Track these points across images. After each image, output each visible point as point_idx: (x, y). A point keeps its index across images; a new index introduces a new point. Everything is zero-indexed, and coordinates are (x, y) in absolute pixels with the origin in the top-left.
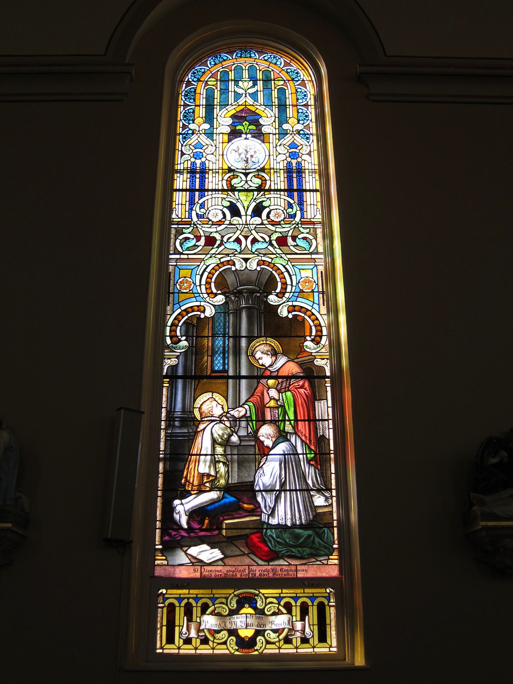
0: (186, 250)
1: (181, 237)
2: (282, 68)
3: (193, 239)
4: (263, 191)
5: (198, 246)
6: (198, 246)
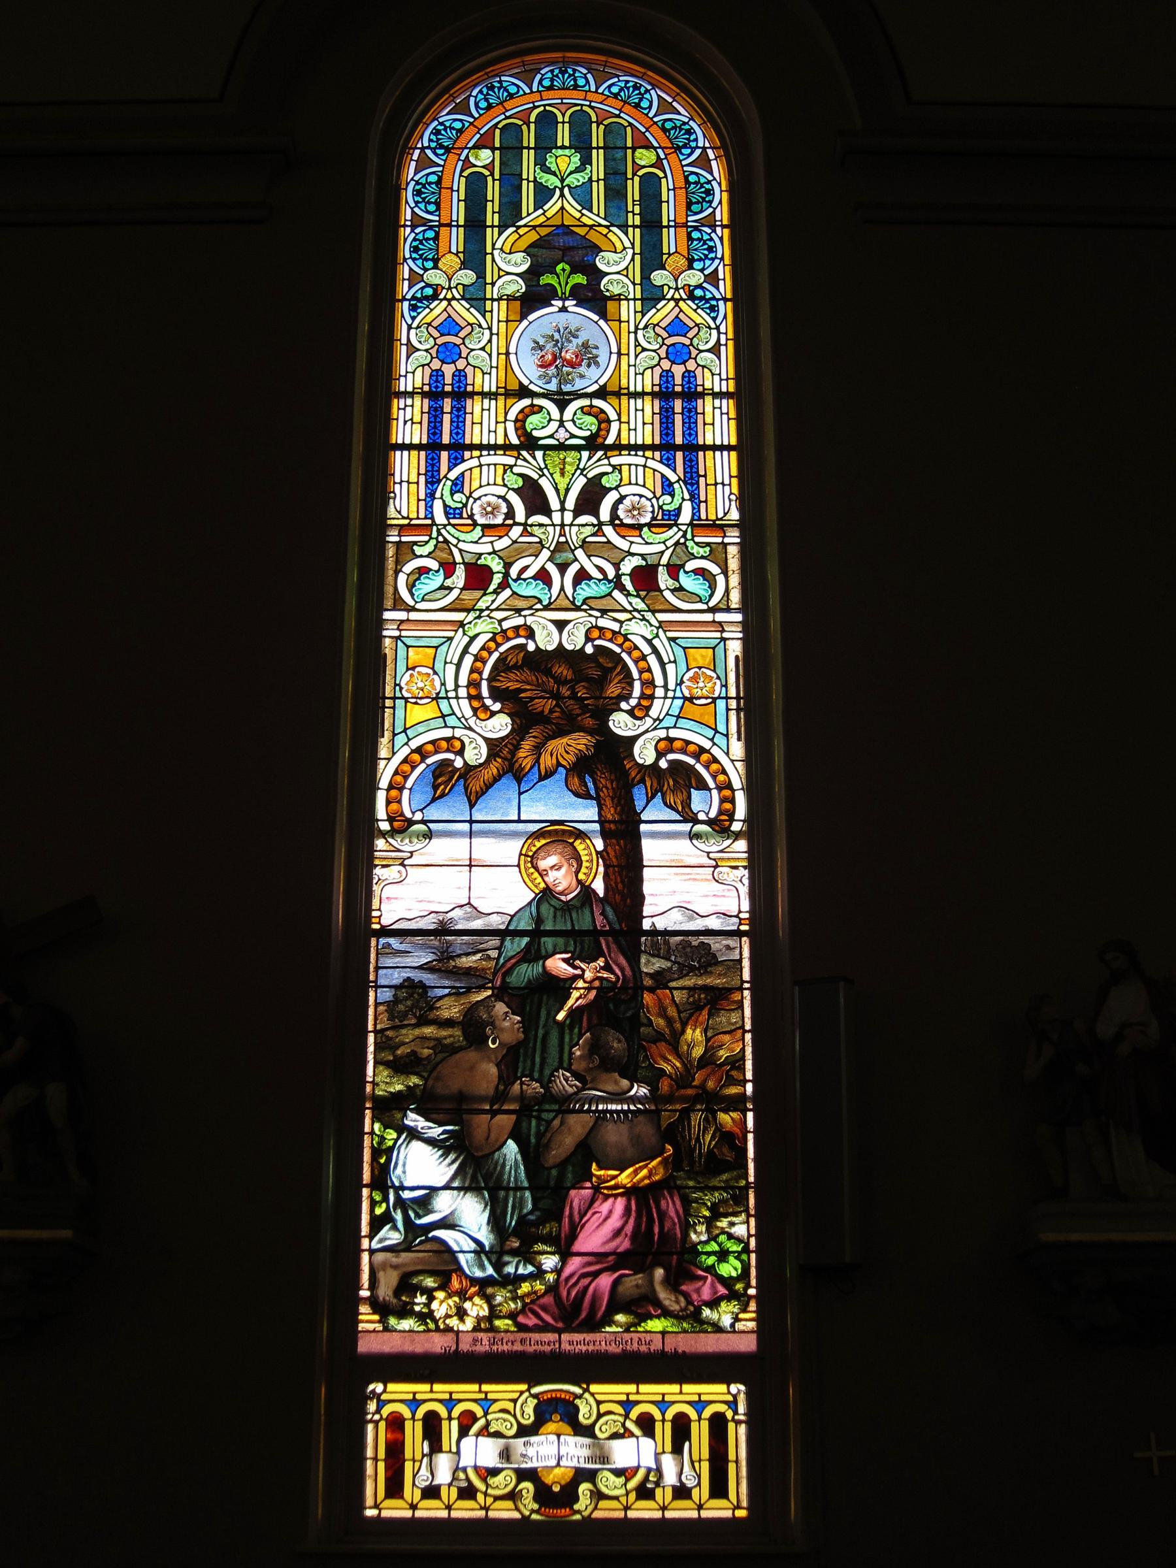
0: (423, 600)
1: (409, 567)
3: (437, 571)
5: (450, 589)
6: (450, 589)
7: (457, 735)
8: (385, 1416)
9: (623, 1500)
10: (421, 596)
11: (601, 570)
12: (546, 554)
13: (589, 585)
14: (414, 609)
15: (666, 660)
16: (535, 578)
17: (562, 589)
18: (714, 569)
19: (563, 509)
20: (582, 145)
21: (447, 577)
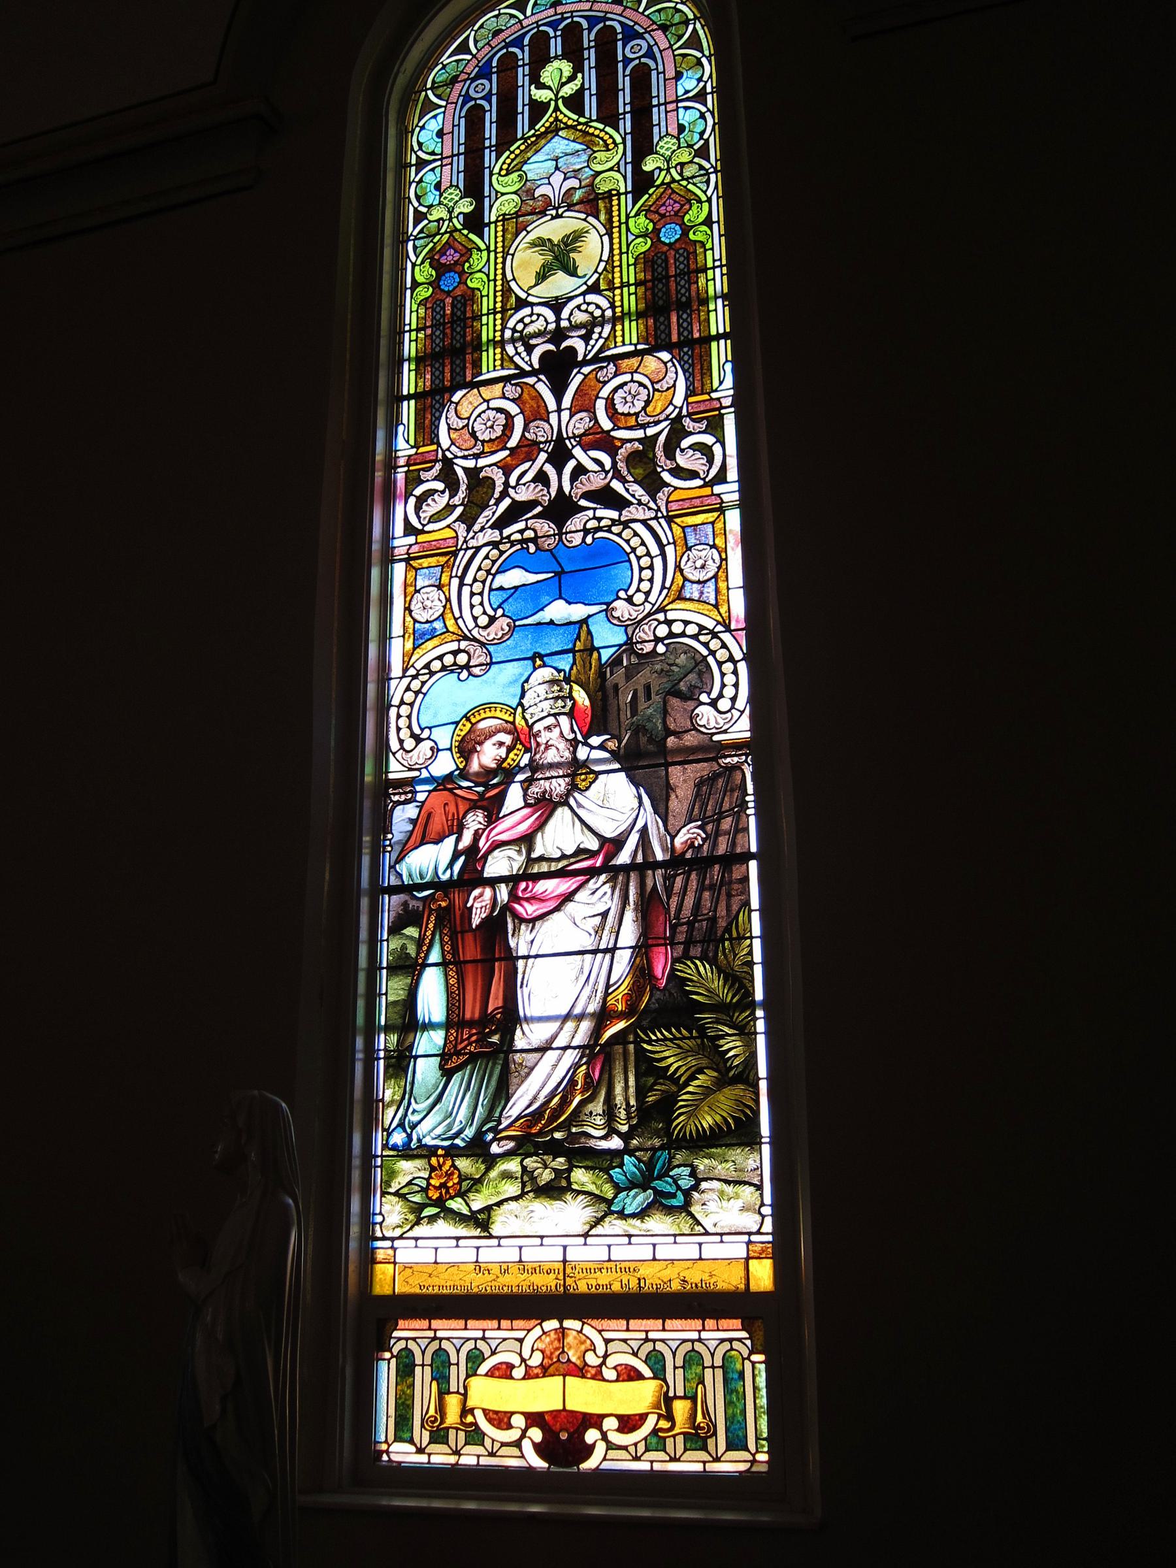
0: (429, 522)
1: (418, 491)
2: (642, 13)
3: (443, 492)
4: (537, 1319)
5: (455, 506)
6: (455, 506)
7: (462, 647)
8: (395, 1354)
9: (632, 1449)
10: (427, 519)
11: (597, 462)
12: (543, 456)
13: (424, 512)
14: (423, 532)
15: (665, 542)
16: (534, 480)
17: (560, 487)
18: (708, 439)
19: (559, 410)
20: (573, 53)
21: (451, 497)
